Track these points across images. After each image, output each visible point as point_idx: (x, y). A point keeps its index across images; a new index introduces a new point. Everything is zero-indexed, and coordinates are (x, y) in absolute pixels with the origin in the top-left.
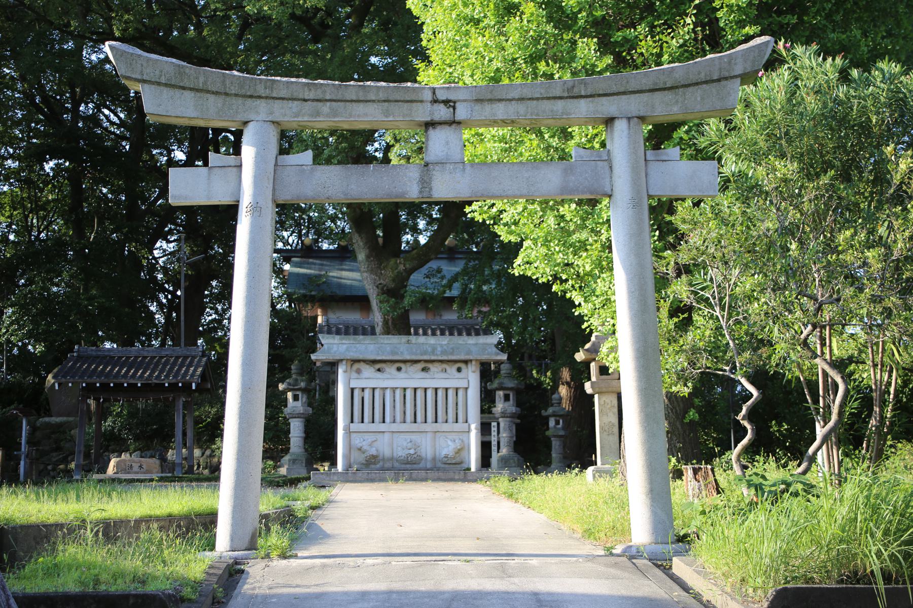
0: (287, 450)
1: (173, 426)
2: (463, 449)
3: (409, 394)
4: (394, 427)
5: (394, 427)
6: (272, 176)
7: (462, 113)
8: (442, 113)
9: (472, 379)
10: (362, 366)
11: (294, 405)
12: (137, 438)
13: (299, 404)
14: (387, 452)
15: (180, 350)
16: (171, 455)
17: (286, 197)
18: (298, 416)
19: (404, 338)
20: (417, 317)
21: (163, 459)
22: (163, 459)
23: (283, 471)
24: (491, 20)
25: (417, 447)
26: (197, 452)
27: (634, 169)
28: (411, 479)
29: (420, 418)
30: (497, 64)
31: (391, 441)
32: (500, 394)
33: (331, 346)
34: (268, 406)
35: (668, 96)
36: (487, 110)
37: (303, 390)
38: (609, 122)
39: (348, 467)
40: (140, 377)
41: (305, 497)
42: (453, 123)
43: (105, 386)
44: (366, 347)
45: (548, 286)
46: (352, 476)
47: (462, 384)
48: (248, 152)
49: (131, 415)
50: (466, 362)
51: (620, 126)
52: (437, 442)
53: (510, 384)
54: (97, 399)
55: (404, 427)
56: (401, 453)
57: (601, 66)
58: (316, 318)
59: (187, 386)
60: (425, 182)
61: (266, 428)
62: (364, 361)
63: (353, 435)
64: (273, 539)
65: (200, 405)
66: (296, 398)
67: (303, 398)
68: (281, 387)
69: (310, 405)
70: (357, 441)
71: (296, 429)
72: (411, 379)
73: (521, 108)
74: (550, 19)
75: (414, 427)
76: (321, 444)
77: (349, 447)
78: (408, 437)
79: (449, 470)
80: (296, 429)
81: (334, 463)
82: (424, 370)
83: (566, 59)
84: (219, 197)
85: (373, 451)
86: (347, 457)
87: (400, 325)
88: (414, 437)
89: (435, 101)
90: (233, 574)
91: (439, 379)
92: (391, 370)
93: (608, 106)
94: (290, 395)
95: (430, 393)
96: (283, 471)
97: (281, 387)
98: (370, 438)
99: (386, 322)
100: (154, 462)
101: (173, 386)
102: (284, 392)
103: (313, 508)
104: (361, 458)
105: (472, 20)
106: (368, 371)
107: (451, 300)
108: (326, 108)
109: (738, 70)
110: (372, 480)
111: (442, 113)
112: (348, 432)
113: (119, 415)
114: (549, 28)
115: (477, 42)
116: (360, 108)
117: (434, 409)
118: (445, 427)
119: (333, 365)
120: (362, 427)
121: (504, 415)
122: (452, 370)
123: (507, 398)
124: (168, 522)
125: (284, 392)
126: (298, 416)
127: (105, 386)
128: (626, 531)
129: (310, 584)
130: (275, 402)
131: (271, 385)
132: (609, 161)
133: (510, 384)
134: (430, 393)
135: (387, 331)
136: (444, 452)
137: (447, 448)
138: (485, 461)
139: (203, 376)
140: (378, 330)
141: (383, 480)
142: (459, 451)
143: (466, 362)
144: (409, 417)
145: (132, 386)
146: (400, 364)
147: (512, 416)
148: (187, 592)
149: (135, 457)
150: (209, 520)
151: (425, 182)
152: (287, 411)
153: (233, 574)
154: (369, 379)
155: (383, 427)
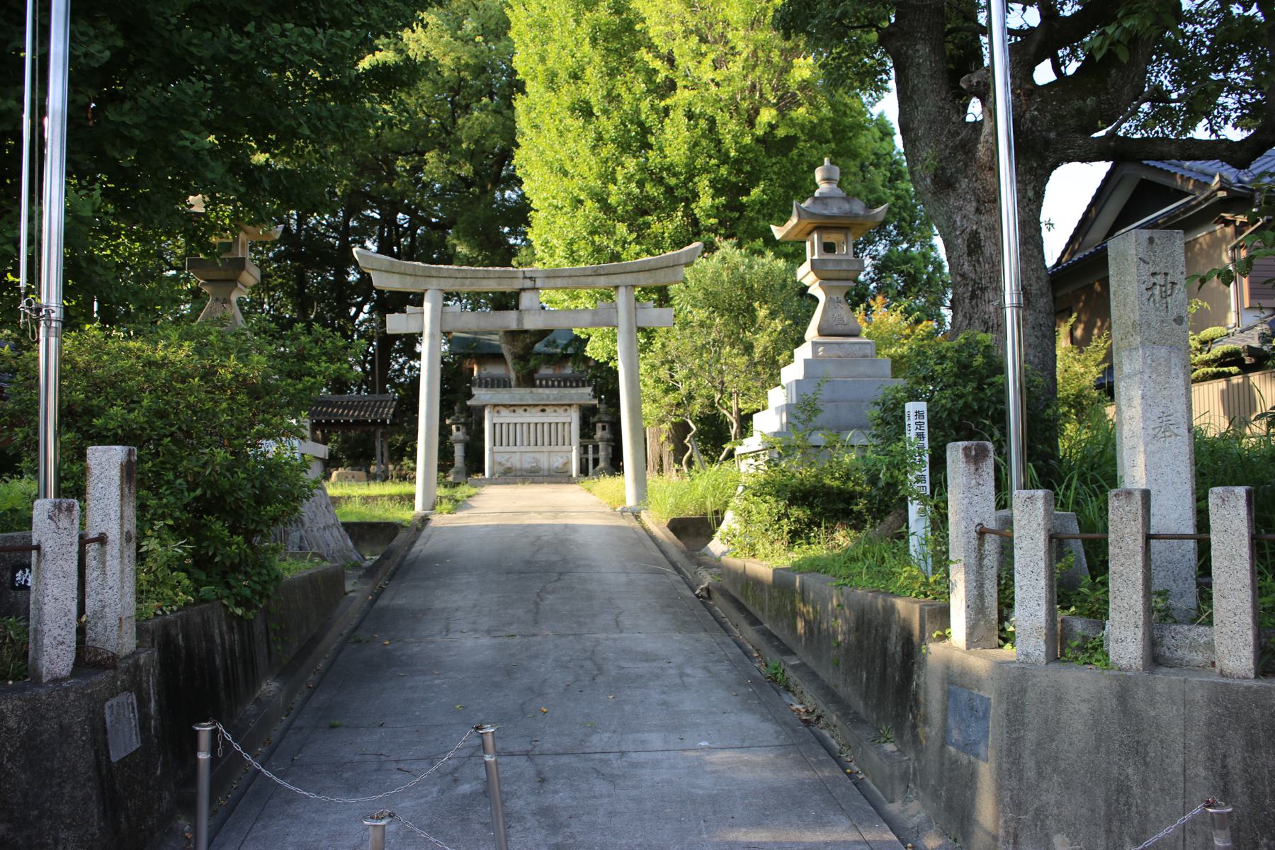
0: (452, 465)
1: (374, 449)
2: (568, 463)
3: (532, 427)
4: (523, 449)
5: (523, 449)
6: (440, 316)
7: (538, 284)
8: (528, 284)
9: (574, 417)
10: (500, 408)
11: (457, 434)
12: (348, 458)
13: (460, 433)
14: (518, 465)
15: (377, 396)
16: (373, 469)
17: (447, 329)
18: (460, 442)
19: (528, 390)
20: (545, 371)
21: (368, 472)
22: (368, 472)
23: (450, 479)
24: (568, 209)
25: (537, 461)
26: (391, 467)
27: (629, 313)
28: (534, 482)
29: (539, 442)
30: (571, 236)
31: (520, 457)
32: (599, 425)
33: (481, 395)
34: (440, 434)
35: (647, 274)
36: (552, 282)
37: (463, 424)
38: (617, 287)
39: (492, 474)
40: (352, 415)
41: (463, 491)
42: (535, 289)
43: (328, 422)
44: (503, 395)
45: (607, 363)
46: (493, 481)
47: (567, 420)
48: (427, 306)
49: (345, 441)
50: (570, 405)
51: (622, 290)
52: (550, 458)
53: (606, 418)
54: (323, 432)
55: (529, 449)
56: (527, 466)
57: (630, 238)
58: (472, 370)
59: (384, 421)
60: (520, 321)
61: (440, 451)
62: (504, 406)
63: (1153, 542)
64: (444, 506)
65: (391, 434)
66: (458, 429)
67: (463, 429)
68: (448, 422)
69: (468, 434)
70: (498, 458)
71: (459, 451)
72: (534, 417)
73: (570, 281)
74: (601, 209)
75: (536, 448)
76: (475, 462)
77: (493, 461)
78: (532, 455)
79: (559, 476)
80: (459, 451)
81: (483, 471)
82: (543, 411)
83: (610, 233)
84: (412, 329)
85: (509, 465)
86: (491, 468)
87: (528, 380)
88: (536, 455)
89: (525, 278)
90: (425, 520)
91: (551, 417)
92: (520, 411)
93: (616, 280)
94: (454, 427)
95: (546, 426)
96: (450, 479)
97: (448, 422)
98: (506, 456)
99: (518, 378)
100: (363, 473)
101: (374, 421)
102: (450, 425)
103: (469, 497)
104: (501, 469)
105: (557, 207)
106: (504, 412)
107: (570, 355)
108: (467, 282)
109: (683, 261)
110: (508, 483)
111: (528, 284)
112: (492, 452)
113: (336, 441)
114: (601, 215)
115: (561, 220)
116: (485, 282)
117: (553, 436)
118: (557, 448)
119: (481, 409)
120: (502, 449)
121: (602, 440)
122: (561, 410)
123: (604, 428)
124: (391, 497)
125: (450, 425)
126: (460, 442)
127: (328, 422)
128: (624, 501)
129: (463, 523)
130: (444, 432)
131: (442, 420)
132: (616, 308)
133: (606, 418)
134: (546, 426)
135: (519, 385)
136: (556, 464)
137: (557, 462)
138: (584, 471)
139: (394, 415)
140: (513, 383)
141: (515, 483)
142: (565, 464)
143: (570, 405)
144: (532, 442)
145: (347, 422)
146: (526, 407)
147: (608, 440)
148: (405, 524)
149: (348, 470)
150: (411, 497)
151: (520, 321)
152: (452, 438)
153: (425, 520)
154: (506, 417)
155: (515, 449)
